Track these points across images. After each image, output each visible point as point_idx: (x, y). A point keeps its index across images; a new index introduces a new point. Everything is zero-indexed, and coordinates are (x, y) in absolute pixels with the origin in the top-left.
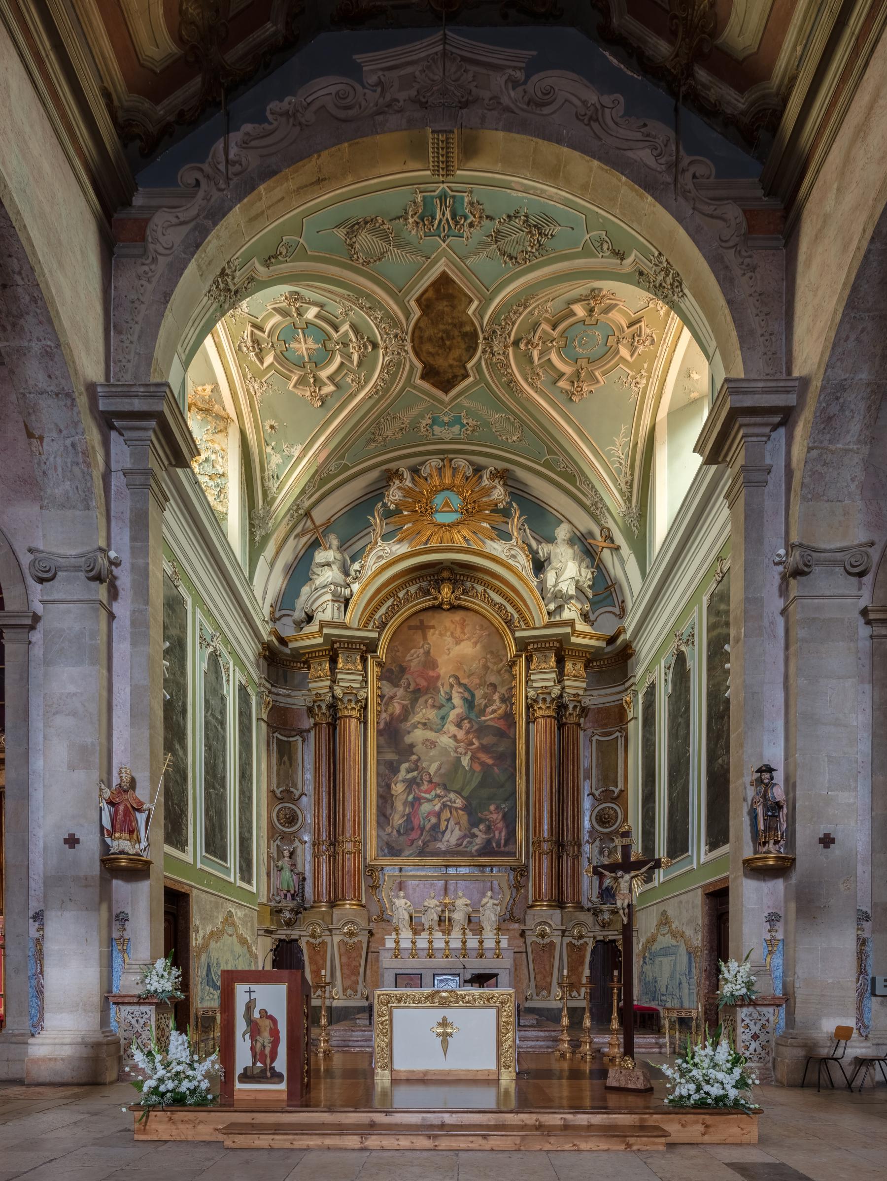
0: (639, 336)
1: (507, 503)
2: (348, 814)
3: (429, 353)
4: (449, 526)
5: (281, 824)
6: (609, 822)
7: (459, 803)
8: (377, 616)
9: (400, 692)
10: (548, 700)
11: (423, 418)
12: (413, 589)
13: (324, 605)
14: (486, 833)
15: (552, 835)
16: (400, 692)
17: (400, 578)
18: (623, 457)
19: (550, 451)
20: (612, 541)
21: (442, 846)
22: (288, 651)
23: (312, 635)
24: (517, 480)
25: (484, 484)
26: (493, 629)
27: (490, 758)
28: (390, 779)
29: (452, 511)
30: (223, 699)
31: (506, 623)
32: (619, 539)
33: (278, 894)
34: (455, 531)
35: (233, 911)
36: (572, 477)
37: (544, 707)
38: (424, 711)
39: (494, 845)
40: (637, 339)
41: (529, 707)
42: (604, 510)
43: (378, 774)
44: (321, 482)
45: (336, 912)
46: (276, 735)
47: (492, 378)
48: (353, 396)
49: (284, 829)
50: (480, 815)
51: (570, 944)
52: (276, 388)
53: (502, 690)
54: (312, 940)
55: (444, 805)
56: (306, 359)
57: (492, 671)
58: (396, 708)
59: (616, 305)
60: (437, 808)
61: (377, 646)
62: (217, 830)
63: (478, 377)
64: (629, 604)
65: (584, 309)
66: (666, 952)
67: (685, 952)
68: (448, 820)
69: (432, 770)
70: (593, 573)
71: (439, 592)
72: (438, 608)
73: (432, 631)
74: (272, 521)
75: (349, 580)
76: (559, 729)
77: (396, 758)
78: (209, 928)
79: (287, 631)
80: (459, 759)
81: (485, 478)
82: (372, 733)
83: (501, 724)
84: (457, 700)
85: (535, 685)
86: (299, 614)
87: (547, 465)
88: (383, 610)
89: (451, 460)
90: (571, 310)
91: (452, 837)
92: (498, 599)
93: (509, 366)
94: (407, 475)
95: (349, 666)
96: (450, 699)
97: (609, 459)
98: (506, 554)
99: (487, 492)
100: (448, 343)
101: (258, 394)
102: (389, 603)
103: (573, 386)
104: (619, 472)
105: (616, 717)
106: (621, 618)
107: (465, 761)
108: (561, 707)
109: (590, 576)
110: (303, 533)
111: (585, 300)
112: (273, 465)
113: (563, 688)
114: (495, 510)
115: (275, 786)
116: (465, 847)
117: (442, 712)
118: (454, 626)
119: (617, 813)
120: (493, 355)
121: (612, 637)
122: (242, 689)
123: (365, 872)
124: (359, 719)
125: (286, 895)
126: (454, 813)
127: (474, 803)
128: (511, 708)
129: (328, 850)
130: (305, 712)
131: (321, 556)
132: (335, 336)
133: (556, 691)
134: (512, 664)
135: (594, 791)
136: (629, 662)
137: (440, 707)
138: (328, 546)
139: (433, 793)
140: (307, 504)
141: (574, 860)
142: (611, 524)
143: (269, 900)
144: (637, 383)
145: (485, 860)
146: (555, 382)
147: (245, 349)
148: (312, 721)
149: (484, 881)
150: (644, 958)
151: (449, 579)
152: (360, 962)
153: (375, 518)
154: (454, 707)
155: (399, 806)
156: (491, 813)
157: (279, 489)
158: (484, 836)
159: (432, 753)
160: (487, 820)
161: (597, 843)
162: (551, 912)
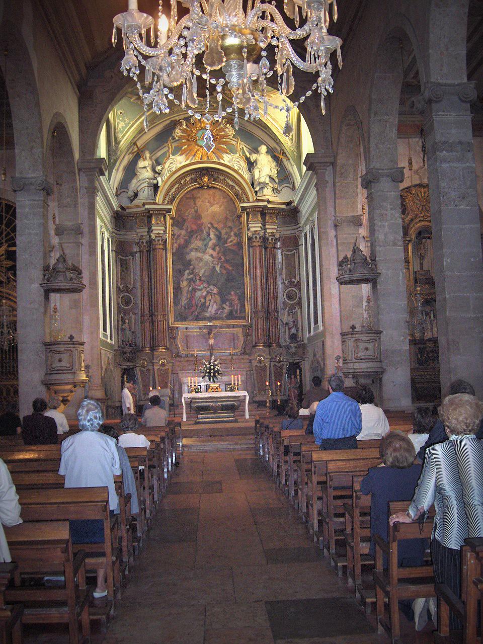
9: (183, 232)
12: (188, 179)
14: (229, 307)
21: (208, 315)
45: (155, 353)
46: (119, 256)
49: (125, 307)
55: (208, 293)
58: (181, 241)
60: (204, 294)
68: (210, 300)
72: (202, 187)
73: (198, 199)
79: (126, 203)
80: (214, 267)
82: (169, 256)
84: (212, 236)
86: (131, 193)
88: (173, 190)
91: (212, 310)
98: (233, 161)
102: (177, 186)
105: (292, 243)
107: (218, 268)
109: (276, 172)
112: (120, 127)
116: (220, 314)
117: (205, 242)
131: (141, 164)
139: (202, 286)
154: (211, 240)
157: (123, 137)
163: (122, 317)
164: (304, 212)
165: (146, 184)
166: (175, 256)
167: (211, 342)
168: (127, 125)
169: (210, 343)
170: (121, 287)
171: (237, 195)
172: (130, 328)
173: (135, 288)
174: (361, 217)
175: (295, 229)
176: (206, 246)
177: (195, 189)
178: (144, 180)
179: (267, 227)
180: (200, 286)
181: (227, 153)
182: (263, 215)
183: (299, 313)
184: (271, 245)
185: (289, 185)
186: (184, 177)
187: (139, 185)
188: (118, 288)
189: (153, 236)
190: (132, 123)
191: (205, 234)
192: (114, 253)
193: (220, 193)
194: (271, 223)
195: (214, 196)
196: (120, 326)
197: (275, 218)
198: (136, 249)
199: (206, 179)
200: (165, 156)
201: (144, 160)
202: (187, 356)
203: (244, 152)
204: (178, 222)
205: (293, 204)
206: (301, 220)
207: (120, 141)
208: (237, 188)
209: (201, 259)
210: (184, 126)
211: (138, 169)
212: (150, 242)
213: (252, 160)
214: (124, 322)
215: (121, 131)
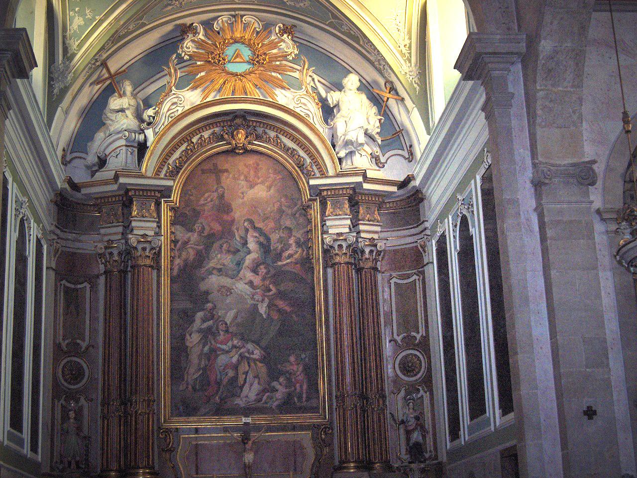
4: (240, 75)
5: (66, 380)
7: (257, 354)
8: (171, 161)
9: (194, 237)
12: (206, 134)
14: (286, 387)
21: (240, 402)
31: (299, 167)
38: (219, 256)
46: (63, 282)
53: (298, 234)
55: (242, 357)
60: (235, 360)
68: (246, 373)
70: (380, 120)
72: (232, 152)
73: (225, 174)
79: (80, 176)
82: (165, 281)
83: (297, 269)
84: (252, 245)
86: (92, 159)
88: (177, 155)
91: (251, 392)
96: (245, 243)
98: (295, 99)
102: (183, 147)
105: (414, 258)
107: (263, 309)
109: (378, 124)
112: (75, 26)
116: (266, 403)
117: (237, 257)
125: (70, 463)
131: (115, 103)
139: (230, 344)
154: (249, 252)
155: (194, 358)
157: (80, 46)
158: (284, 390)
160: (287, 372)
163: (63, 406)
164: (434, 199)
167: (249, 457)
168: (88, 22)
169: (247, 461)
170: (64, 345)
171: (301, 166)
172: (79, 429)
173: (93, 346)
174: (595, 167)
175: (414, 235)
176: (239, 264)
177: (218, 154)
178: (119, 133)
179: (362, 227)
181: (283, 88)
182: (354, 204)
183: (427, 401)
184: (369, 264)
185: (400, 152)
186: (198, 129)
187: (110, 144)
188: (57, 347)
189: (133, 240)
190: (98, 18)
192: (52, 274)
193: (270, 162)
194: (369, 221)
195: (256, 169)
196: (58, 427)
197: (376, 212)
199: (241, 135)
200: (164, 91)
201: (121, 97)
203: (315, 89)
204: (181, 218)
205: (412, 184)
206: (428, 213)
207: (74, 55)
208: (302, 153)
209: (229, 290)
210: (201, 36)
211: (109, 115)
212: (128, 252)
213: (330, 101)
215: (76, 35)
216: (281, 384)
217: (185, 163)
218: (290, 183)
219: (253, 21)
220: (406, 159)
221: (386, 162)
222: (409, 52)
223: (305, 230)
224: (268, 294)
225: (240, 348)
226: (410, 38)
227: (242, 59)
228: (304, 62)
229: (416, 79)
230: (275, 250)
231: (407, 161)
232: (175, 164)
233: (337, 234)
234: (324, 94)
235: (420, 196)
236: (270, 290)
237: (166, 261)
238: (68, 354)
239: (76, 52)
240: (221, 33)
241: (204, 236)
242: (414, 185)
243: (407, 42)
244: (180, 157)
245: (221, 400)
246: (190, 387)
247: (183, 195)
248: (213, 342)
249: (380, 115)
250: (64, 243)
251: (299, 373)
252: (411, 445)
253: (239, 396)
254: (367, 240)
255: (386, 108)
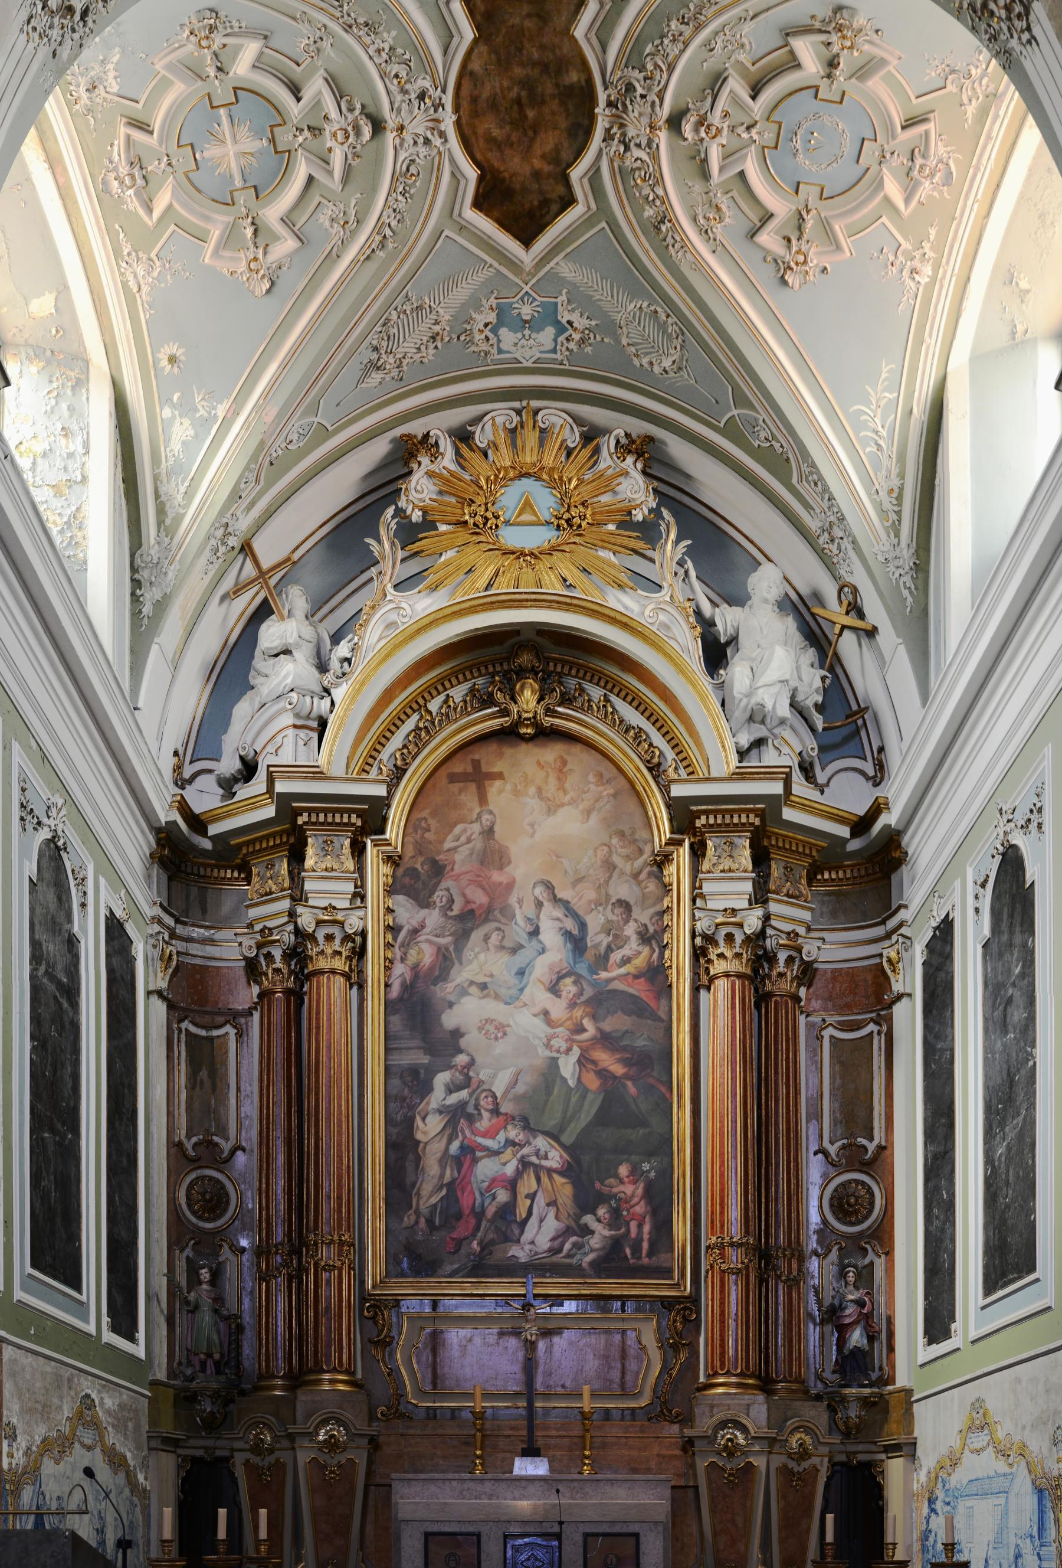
0: (924, 156)
1: (651, 511)
2: (325, 1184)
3: (491, 140)
4: (532, 554)
5: (194, 1213)
6: (856, 1212)
7: (555, 1158)
8: (385, 755)
9: (433, 918)
10: (739, 938)
11: (478, 308)
12: (458, 693)
13: (279, 739)
14: (610, 1226)
15: (747, 1232)
16: (433, 918)
17: (432, 667)
18: (884, 433)
19: (741, 400)
20: (861, 615)
21: (520, 1253)
22: (207, 844)
23: (252, 804)
24: (671, 466)
25: (602, 466)
26: (623, 781)
27: (619, 1061)
28: (412, 1108)
29: (538, 523)
30: (72, 943)
31: (650, 769)
32: (876, 612)
33: (189, 1363)
34: (542, 566)
35: (94, 1396)
36: (780, 462)
37: (729, 954)
38: (482, 957)
39: (628, 1251)
40: (919, 161)
41: (699, 954)
42: (846, 544)
43: (387, 1097)
44: (270, 469)
45: (303, 1397)
46: (185, 1025)
47: (622, 207)
48: (332, 258)
49: (201, 1224)
50: (597, 1185)
51: (785, 1472)
52: (178, 266)
53: (643, 916)
54: (255, 1460)
55: (525, 1164)
56: (238, 183)
57: (622, 873)
58: (425, 954)
59: (883, 62)
60: (510, 1170)
61: (385, 819)
62: (58, 1220)
63: (593, 206)
64: (894, 758)
65: (818, 55)
66: (980, 1489)
67: (1029, 1486)
68: (532, 1197)
69: (499, 1089)
70: (823, 678)
71: (514, 699)
72: (509, 735)
73: (498, 783)
74: (176, 565)
75: (328, 679)
76: (758, 1006)
77: (425, 1060)
78: (40, 1431)
79: (204, 797)
80: (553, 1063)
81: (605, 453)
82: (375, 1008)
83: (639, 989)
84: (550, 935)
85: (711, 905)
86: (229, 765)
87: (730, 431)
88: (396, 741)
89: (536, 412)
90: (792, 52)
91: (540, 1234)
92: (633, 717)
93: (660, 180)
94: (446, 446)
95: (329, 862)
96: (535, 933)
97: (857, 435)
98: (650, 611)
99: (607, 484)
100: (531, 114)
101: (145, 289)
102: (410, 724)
103: (789, 248)
104: (877, 465)
106: (876, 785)
107: (568, 1068)
108: (759, 954)
109: (818, 683)
110: (238, 590)
111: (820, 31)
112: (176, 446)
113: (767, 918)
114: (627, 524)
115: (183, 1132)
116: (569, 1256)
117: (520, 960)
118: (541, 774)
119: (872, 1195)
120: (627, 148)
121: (862, 819)
122: (115, 929)
123: (361, 1310)
124: (347, 976)
125: (203, 1364)
126: (545, 1179)
127: (586, 1159)
128: (661, 956)
129: (286, 1264)
130: (242, 973)
131: (271, 634)
132: (295, 110)
133: (753, 921)
134: (662, 861)
135: (826, 1144)
136: (894, 878)
137: (515, 950)
138: (285, 613)
139: (501, 1137)
140: (244, 524)
141: (790, 1288)
142: (859, 578)
143: (171, 1374)
144: (914, 271)
145: (611, 1287)
146: (753, 234)
147: (116, 184)
148: (256, 990)
149: (607, 1331)
150: (931, 1501)
151: (534, 671)
152: (351, 1505)
153: (379, 541)
154: (543, 951)
155: (431, 1165)
156: (622, 1182)
157: (189, 494)
158: (607, 1233)
159: (501, 1048)
160: (614, 1196)
161: (834, 1255)
162: (747, 1399)
165: (288, 719)
166: (395, 1012)
180: (493, 1137)
188: (175, 1147)
190: (221, 411)
191: (519, 929)
194: (788, 895)
197: (804, 881)
198: (247, 995)
199: (528, 699)
202: (432, 1414)
207: (179, 519)
213: (720, 627)
214: (194, 1280)
216: (599, 1220)
217: (414, 758)
218: (632, 805)
219: (561, 422)
220: (868, 778)
221: (828, 784)
222: (896, 509)
223: (658, 908)
224: (578, 1037)
225: (522, 1146)
226: (902, 476)
227: (536, 515)
228: (668, 526)
229: (907, 579)
230: (596, 946)
231: (870, 783)
232: (393, 761)
233: (725, 910)
234: (707, 609)
235: (897, 854)
236: (584, 1030)
237: (376, 967)
238: (195, 1162)
239: (182, 511)
240: (490, 452)
241: (451, 917)
242: (888, 822)
243: (896, 482)
244: (405, 746)
245: (483, 1249)
246: (422, 1220)
247: (410, 830)
248: (467, 1133)
249: (822, 667)
250: (181, 946)
251: (636, 1200)
252: (846, 1352)
253: (518, 1241)
254: (784, 936)
255: (835, 661)
